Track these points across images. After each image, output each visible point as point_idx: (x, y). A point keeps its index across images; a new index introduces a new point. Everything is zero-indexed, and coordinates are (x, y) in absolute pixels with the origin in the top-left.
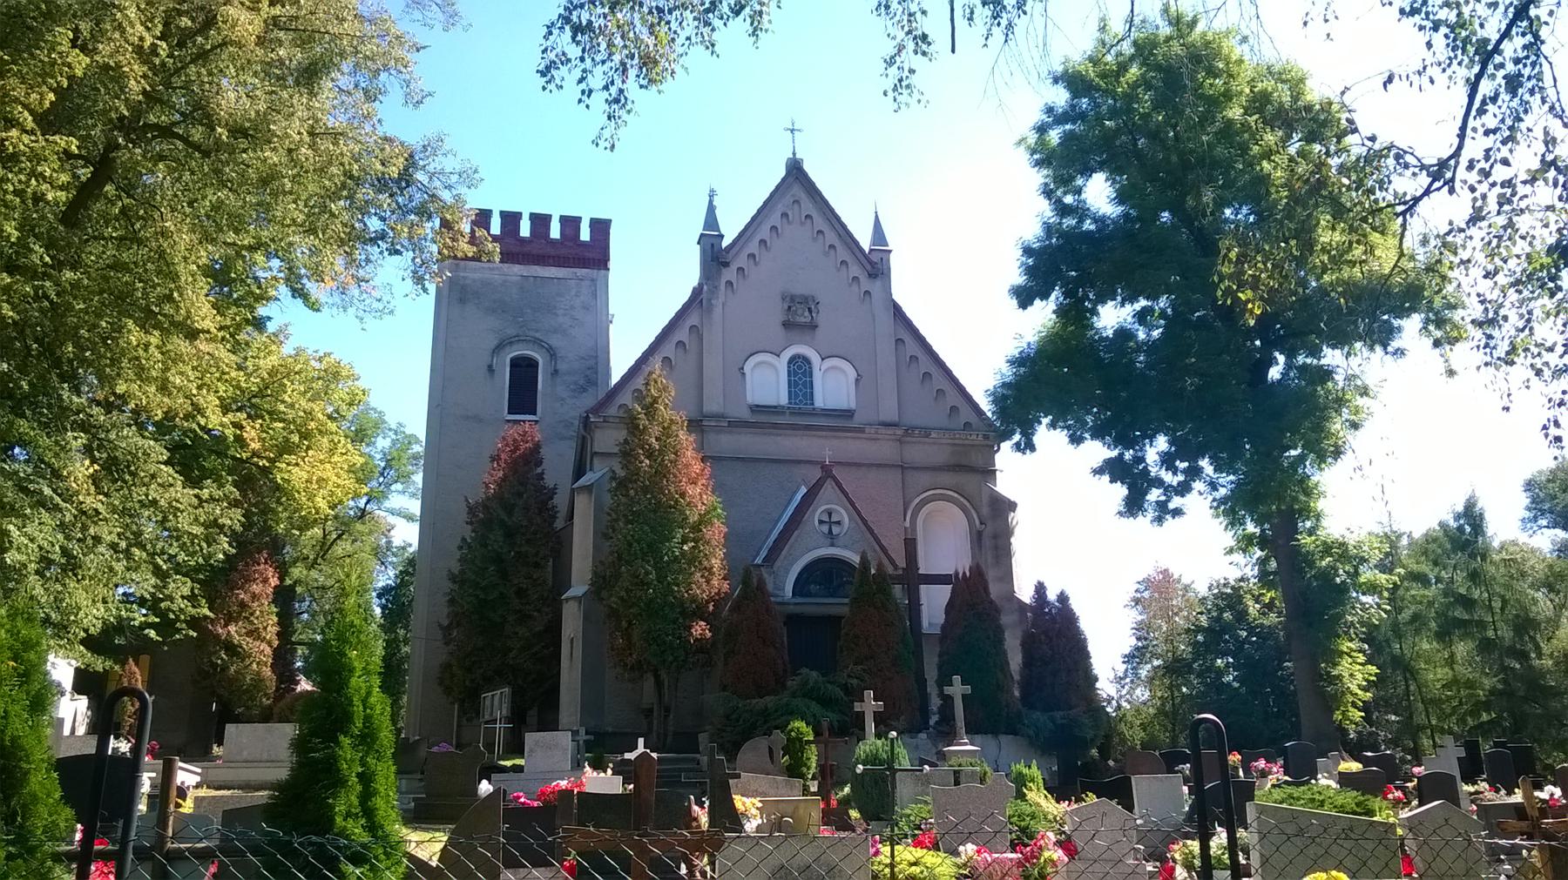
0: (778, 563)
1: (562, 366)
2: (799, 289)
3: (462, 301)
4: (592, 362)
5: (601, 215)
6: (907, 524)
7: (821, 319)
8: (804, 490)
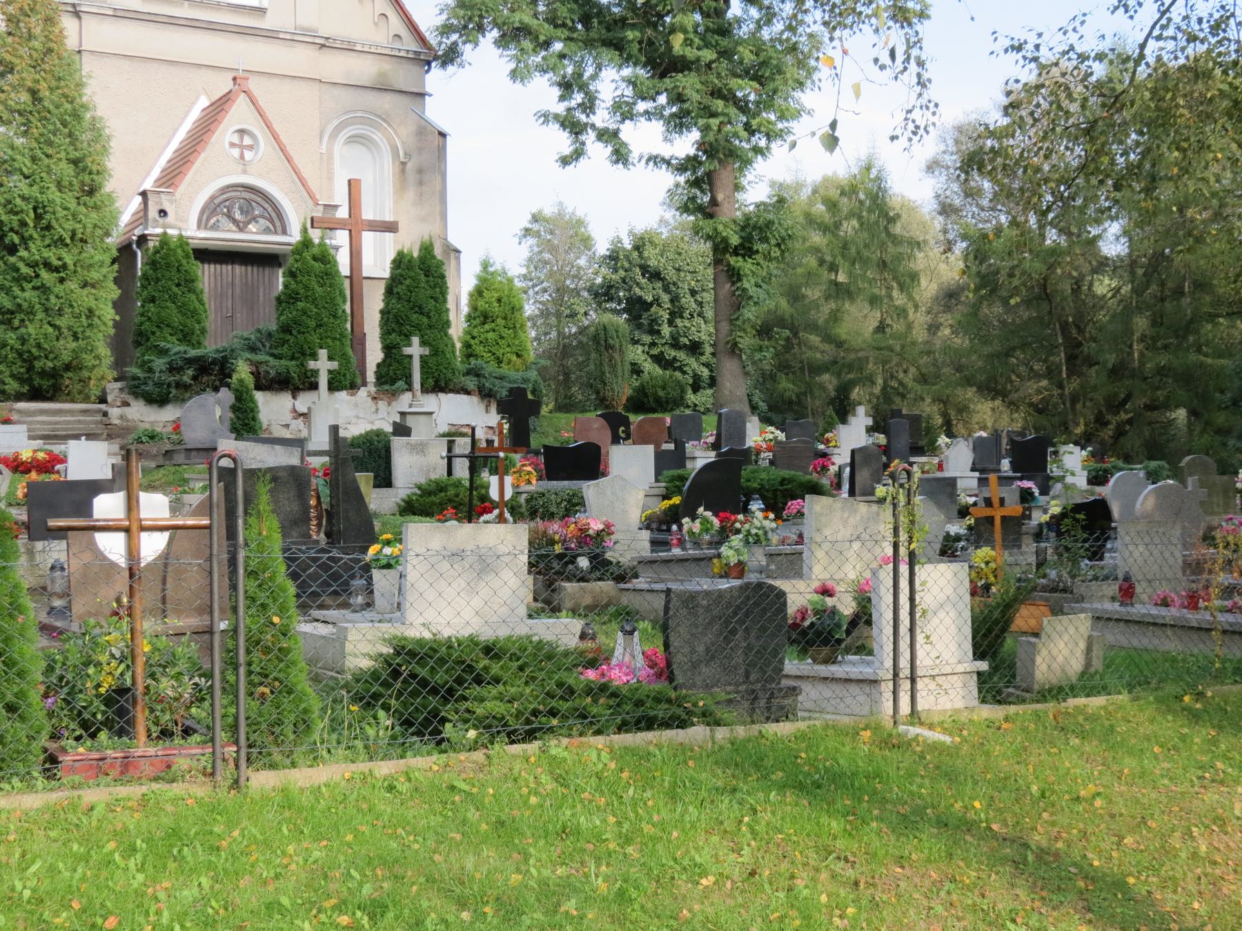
8: (204, 102)
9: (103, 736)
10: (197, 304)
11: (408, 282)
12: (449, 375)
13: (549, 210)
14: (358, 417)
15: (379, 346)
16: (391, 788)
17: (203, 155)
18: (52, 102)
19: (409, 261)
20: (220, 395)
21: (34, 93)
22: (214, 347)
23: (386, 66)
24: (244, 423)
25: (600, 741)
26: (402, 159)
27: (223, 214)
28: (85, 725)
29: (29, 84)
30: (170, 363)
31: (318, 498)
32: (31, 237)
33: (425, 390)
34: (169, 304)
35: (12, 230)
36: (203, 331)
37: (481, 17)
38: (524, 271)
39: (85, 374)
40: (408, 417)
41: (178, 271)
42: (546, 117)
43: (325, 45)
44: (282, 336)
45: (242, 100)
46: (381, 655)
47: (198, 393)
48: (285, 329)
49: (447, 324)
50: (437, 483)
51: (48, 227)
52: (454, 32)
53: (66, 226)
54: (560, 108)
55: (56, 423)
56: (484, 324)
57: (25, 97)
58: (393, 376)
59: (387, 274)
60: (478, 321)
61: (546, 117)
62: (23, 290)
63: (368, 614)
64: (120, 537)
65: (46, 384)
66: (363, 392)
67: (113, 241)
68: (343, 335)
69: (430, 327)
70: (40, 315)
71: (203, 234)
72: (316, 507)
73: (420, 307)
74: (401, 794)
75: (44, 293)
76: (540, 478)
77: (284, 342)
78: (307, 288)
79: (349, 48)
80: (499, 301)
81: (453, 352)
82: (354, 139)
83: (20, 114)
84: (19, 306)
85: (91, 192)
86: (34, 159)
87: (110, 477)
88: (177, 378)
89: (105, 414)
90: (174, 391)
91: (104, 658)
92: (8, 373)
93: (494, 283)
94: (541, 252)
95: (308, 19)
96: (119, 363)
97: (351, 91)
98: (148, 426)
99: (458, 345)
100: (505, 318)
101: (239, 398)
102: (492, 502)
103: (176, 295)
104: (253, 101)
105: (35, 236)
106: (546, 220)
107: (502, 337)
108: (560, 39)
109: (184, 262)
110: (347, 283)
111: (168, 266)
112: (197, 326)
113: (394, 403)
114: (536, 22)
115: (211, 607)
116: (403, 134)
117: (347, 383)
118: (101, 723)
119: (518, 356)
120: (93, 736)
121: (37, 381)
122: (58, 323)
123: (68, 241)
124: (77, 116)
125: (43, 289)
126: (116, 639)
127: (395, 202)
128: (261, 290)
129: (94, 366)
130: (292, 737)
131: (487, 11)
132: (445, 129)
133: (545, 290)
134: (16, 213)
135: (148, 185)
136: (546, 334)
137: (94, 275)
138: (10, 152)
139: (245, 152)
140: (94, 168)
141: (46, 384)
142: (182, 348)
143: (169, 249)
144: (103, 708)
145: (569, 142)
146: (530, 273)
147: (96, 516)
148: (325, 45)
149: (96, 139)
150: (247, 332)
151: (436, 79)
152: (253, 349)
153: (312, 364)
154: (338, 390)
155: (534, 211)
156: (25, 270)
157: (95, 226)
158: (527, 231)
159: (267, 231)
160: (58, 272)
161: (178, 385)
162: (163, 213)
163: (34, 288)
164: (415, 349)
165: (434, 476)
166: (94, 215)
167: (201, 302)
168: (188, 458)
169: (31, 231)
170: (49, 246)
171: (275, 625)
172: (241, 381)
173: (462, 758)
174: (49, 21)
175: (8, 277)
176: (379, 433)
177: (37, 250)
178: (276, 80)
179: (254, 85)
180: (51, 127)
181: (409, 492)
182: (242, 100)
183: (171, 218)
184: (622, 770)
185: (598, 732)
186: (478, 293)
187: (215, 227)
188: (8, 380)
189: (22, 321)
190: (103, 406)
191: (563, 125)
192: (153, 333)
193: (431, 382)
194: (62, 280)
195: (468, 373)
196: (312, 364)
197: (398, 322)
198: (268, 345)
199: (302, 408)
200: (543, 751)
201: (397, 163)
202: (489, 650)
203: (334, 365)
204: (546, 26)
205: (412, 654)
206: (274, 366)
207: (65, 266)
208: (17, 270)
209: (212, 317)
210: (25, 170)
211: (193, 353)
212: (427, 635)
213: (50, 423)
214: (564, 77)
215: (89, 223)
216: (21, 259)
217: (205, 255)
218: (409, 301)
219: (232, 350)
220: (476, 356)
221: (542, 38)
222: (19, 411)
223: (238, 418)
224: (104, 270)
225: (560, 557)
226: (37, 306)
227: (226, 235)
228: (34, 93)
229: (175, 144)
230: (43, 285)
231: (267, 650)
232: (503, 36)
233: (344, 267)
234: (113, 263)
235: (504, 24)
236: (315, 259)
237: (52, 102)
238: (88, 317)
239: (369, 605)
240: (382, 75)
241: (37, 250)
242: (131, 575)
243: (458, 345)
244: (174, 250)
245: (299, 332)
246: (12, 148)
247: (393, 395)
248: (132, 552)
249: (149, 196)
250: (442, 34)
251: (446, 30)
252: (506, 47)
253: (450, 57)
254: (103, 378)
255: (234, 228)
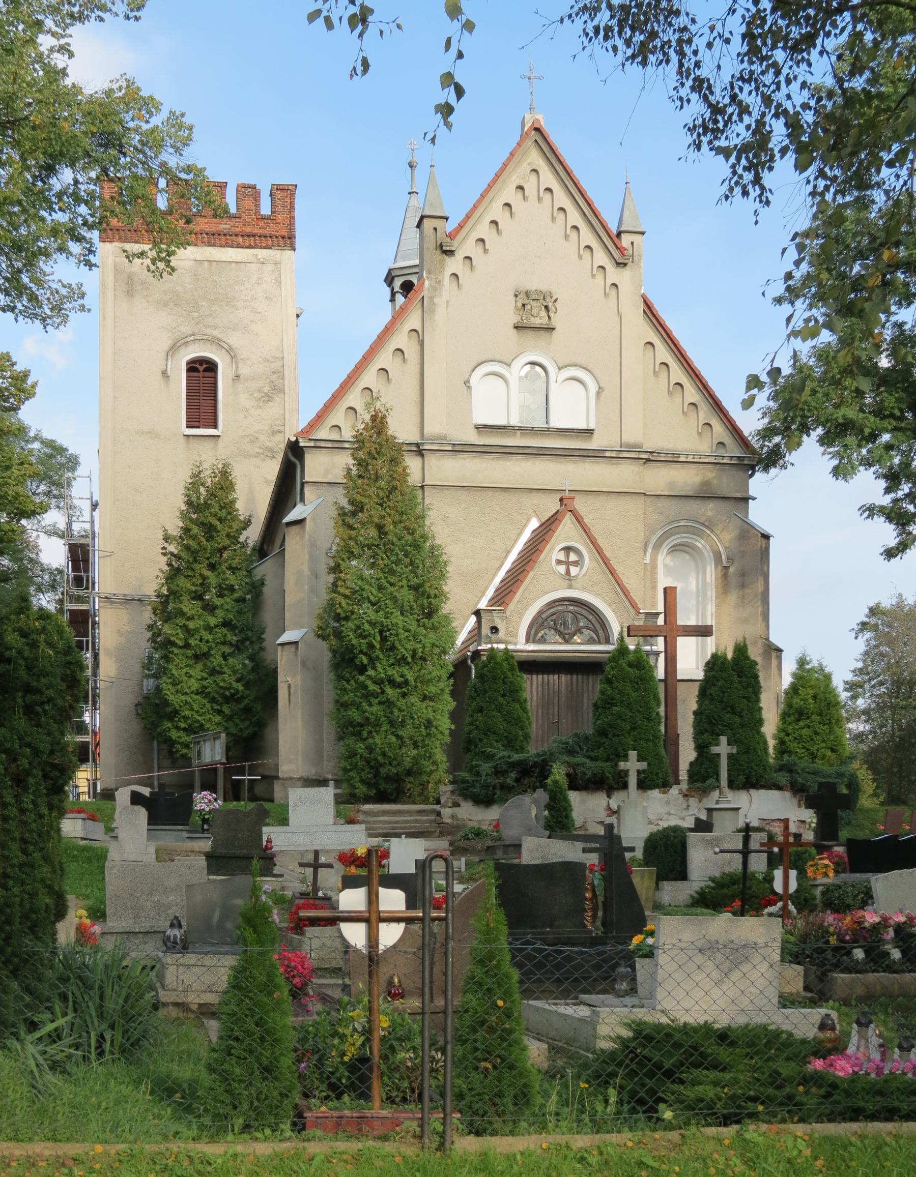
0: (511, 607)
1: (244, 371)
2: (533, 285)
3: (130, 292)
4: (276, 365)
5: (284, 180)
6: (648, 559)
7: (556, 321)
8: (534, 524)
9: (346, 1098)
10: (521, 712)
11: (720, 684)
12: (761, 772)
13: (887, 603)
14: (669, 814)
15: (692, 745)
16: (582, 1160)
17: (531, 574)
18: (396, 534)
19: (723, 663)
20: (535, 795)
21: (380, 528)
22: (535, 752)
23: (710, 474)
24: (558, 822)
25: (800, 1129)
26: (725, 564)
27: (550, 628)
28: (332, 1087)
29: (376, 520)
30: (495, 767)
31: (594, 892)
32: (378, 658)
33: (732, 785)
34: (495, 713)
35: (361, 652)
36: (527, 737)
37: (804, 417)
38: (860, 665)
39: (425, 778)
40: (715, 814)
41: (504, 682)
42: (871, 511)
43: (650, 459)
44: (598, 739)
45: (568, 519)
46: (619, 1037)
47: (519, 794)
48: (602, 733)
49: (760, 722)
50: (730, 875)
51: (393, 648)
52: (776, 435)
53: (408, 647)
54: (886, 500)
55: (396, 822)
56: (799, 720)
57: (373, 532)
58: (703, 776)
59: (700, 675)
60: (792, 718)
61: (871, 511)
62: (370, 705)
63: (628, 1000)
64: (361, 928)
65: (390, 787)
66: (674, 791)
67: (451, 658)
68: (656, 736)
69: (742, 726)
70: (385, 727)
71: (531, 647)
72: (591, 900)
73: (732, 707)
74: (590, 1165)
75: (389, 707)
76: (836, 872)
77: (599, 745)
78: (621, 692)
79: (672, 459)
80: (815, 697)
81: (766, 749)
82: (676, 549)
83: (369, 549)
84: (368, 719)
85: (429, 615)
86: (380, 588)
87: (413, 871)
88: (501, 780)
89: (439, 814)
90: (498, 792)
91: (348, 1032)
92: (357, 779)
93: (810, 680)
94: (877, 646)
95: (633, 434)
96: (455, 767)
97: (674, 502)
98: (475, 825)
99: (771, 743)
100: (820, 714)
101: (553, 798)
102: (775, 893)
103: (501, 705)
104: (579, 519)
105: (381, 656)
106: (884, 613)
107: (817, 733)
108: (887, 431)
109: (509, 674)
110: (661, 687)
111: (494, 678)
112: (520, 733)
113: (705, 800)
114: (861, 415)
115: (423, 990)
116: (724, 539)
117: (660, 782)
118: (346, 1087)
119: (833, 751)
120: (339, 1097)
121: (383, 786)
122: (400, 733)
123: (410, 660)
124: (417, 546)
125: (388, 704)
126: (359, 1016)
127: (718, 606)
128: (585, 696)
129: (432, 771)
130: (511, 1108)
131: (809, 410)
132: (768, 530)
133: (881, 684)
134: (365, 637)
135: (483, 605)
136: (881, 727)
137: (433, 689)
138: (360, 583)
139: (571, 568)
140: (432, 593)
141: (390, 787)
142: (506, 753)
143: (496, 663)
144: (347, 1074)
145: (895, 534)
146: (866, 667)
147: (341, 908)
148: (650, 459)
149: (434, 566)
150: (566, 736)
151: (758, 483)
152: (571, 752)
153: (622, 765)
154: (651, 789)
155: (872, 604)
156: (372, 687)
157: (433, 645)
158: (864, 626)
159: (591, 641)
160: (401, 688)
161: (503, 787)
162: (495, 630)
163: (380, 703)
164: (723, 748)
165: (727, 870)
166: (432, 635)
167: (525, 710)
168: (505, 853)
169: (378, 652)
170: (393, 665)
171: (499, 1008)
172: (555, 782)
173: (657, 1136)
174: (394, 461)
175: (358, 694)
176: (676, 829)
177: (382, 669)
178: (602, 498)
179: (580, 504)
180: (393, 558)
181: (703, 884)
182: (568, 519)
183: (502, 634)
184: (816, 1158)
185: (801, 1120)
186: (794, 689)
187: (543, 640)
188: (358, 785)
189: (370, 732)
190: (437, 807)
191: (889, 518)
192: (481, 740)
193: (742, 778)
194: (404, 695)
195: (781, 768)
196: (622, 765)
197: (710, 722)
198: (585, 748)
199: (614, 806)
200: (739, 1134)
201: (720, 568)
202: (724, 1037)
203: (644, 765)
204: (872, 418)
205: (649, 1038)
206: (590, 767)
207: (406, 682)
208: (366, 687)
209: (534, 725)
210: (372, 598)
211: (516, 757)
212: (664, 1020)
213: (390, 822)
214: (891, 468)
215: (427, 642)
216: (370, 677)
217: (532, 666)
218: (722, 702)
219: (552, 754)
220: (790, 753)
221: (867, 431)
222: (365, 813)
223: (552, 816)
224: (442, 685)
225: (836, 949)
226: (383, 719)
227: (554, 647)
228: (380, 528)
229: (507, 565)
230: (388, 699)
231: (491, 1030)
232: (827, 433)
233: (660, 673)
234: (449, 678)
235: (827, 421)
236: (630, 665)
237: (396, 534)
238: (426, 728)
239: (633, 991)
240: (706, 483)
241: (382, 669)
242: (371, 959)
243: (771, 743)
244: (500, 664)
245: (614, 735)
246: (361, 578)
247: (705, 792)
248: (373, 939)
249: (483, 614)
250: (764, 438)
251: (766, 433)
252: (830, 445)
253: (773, 459)
254: (440, 781)
255: (560, 640)
